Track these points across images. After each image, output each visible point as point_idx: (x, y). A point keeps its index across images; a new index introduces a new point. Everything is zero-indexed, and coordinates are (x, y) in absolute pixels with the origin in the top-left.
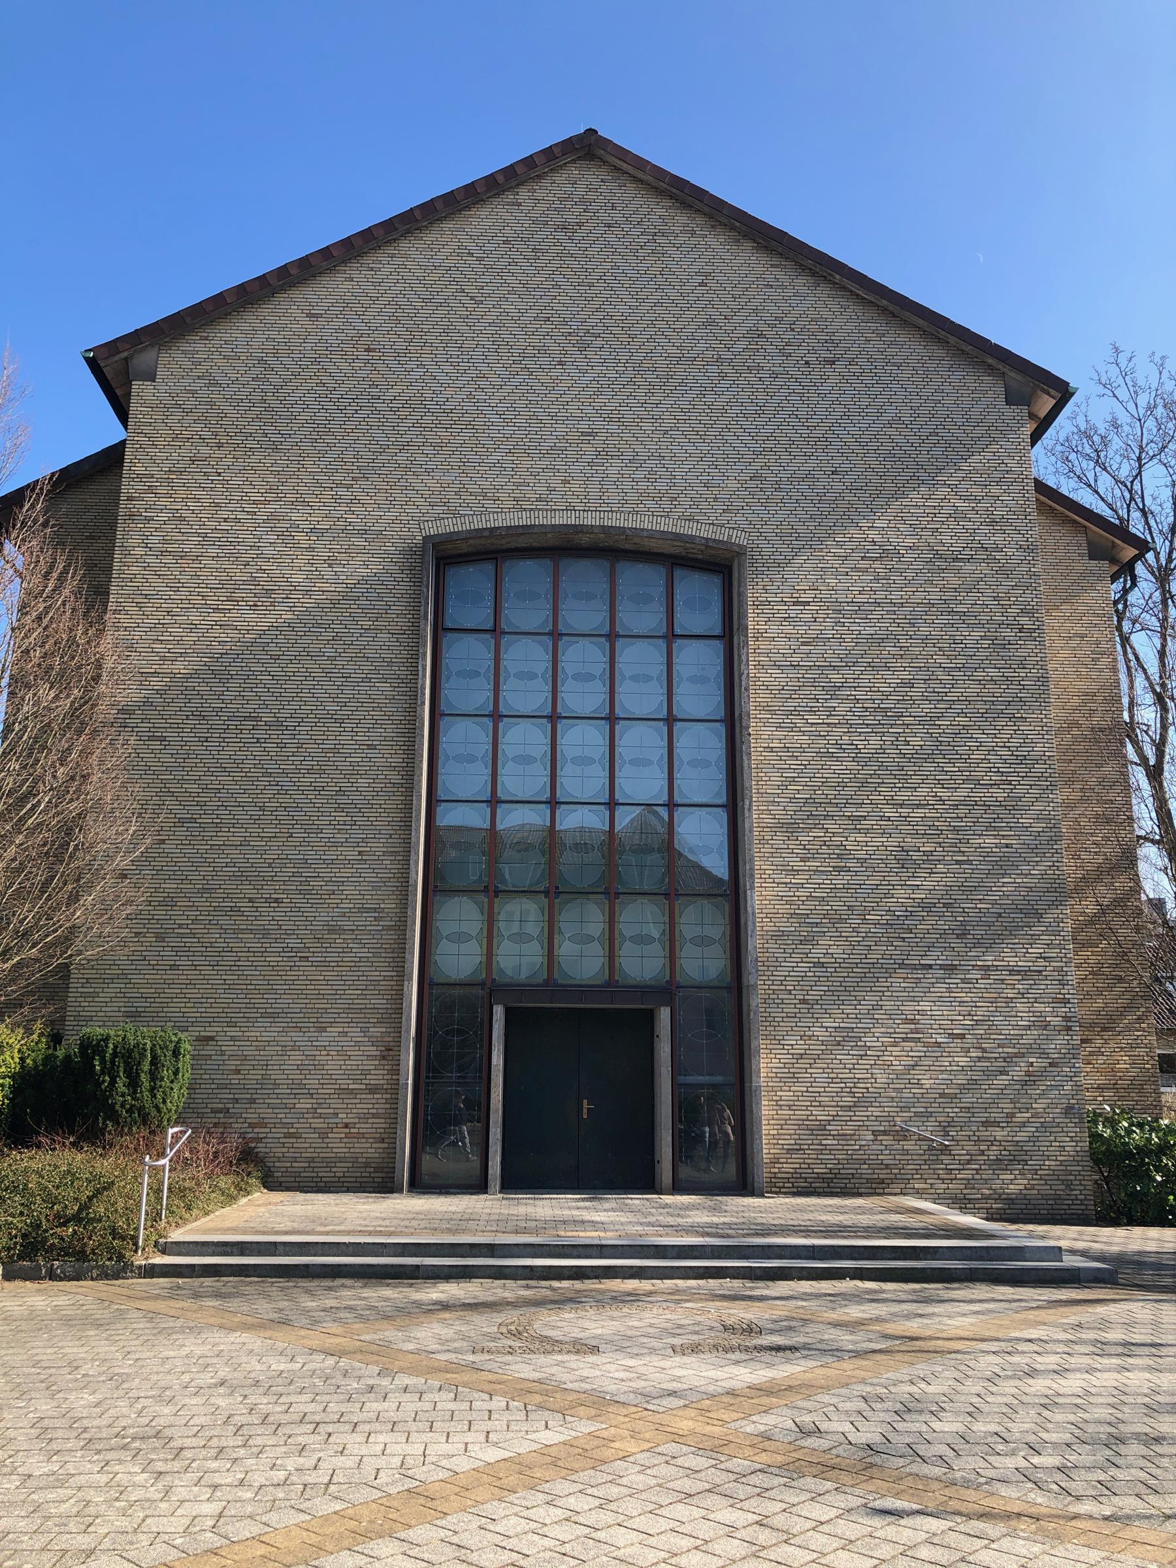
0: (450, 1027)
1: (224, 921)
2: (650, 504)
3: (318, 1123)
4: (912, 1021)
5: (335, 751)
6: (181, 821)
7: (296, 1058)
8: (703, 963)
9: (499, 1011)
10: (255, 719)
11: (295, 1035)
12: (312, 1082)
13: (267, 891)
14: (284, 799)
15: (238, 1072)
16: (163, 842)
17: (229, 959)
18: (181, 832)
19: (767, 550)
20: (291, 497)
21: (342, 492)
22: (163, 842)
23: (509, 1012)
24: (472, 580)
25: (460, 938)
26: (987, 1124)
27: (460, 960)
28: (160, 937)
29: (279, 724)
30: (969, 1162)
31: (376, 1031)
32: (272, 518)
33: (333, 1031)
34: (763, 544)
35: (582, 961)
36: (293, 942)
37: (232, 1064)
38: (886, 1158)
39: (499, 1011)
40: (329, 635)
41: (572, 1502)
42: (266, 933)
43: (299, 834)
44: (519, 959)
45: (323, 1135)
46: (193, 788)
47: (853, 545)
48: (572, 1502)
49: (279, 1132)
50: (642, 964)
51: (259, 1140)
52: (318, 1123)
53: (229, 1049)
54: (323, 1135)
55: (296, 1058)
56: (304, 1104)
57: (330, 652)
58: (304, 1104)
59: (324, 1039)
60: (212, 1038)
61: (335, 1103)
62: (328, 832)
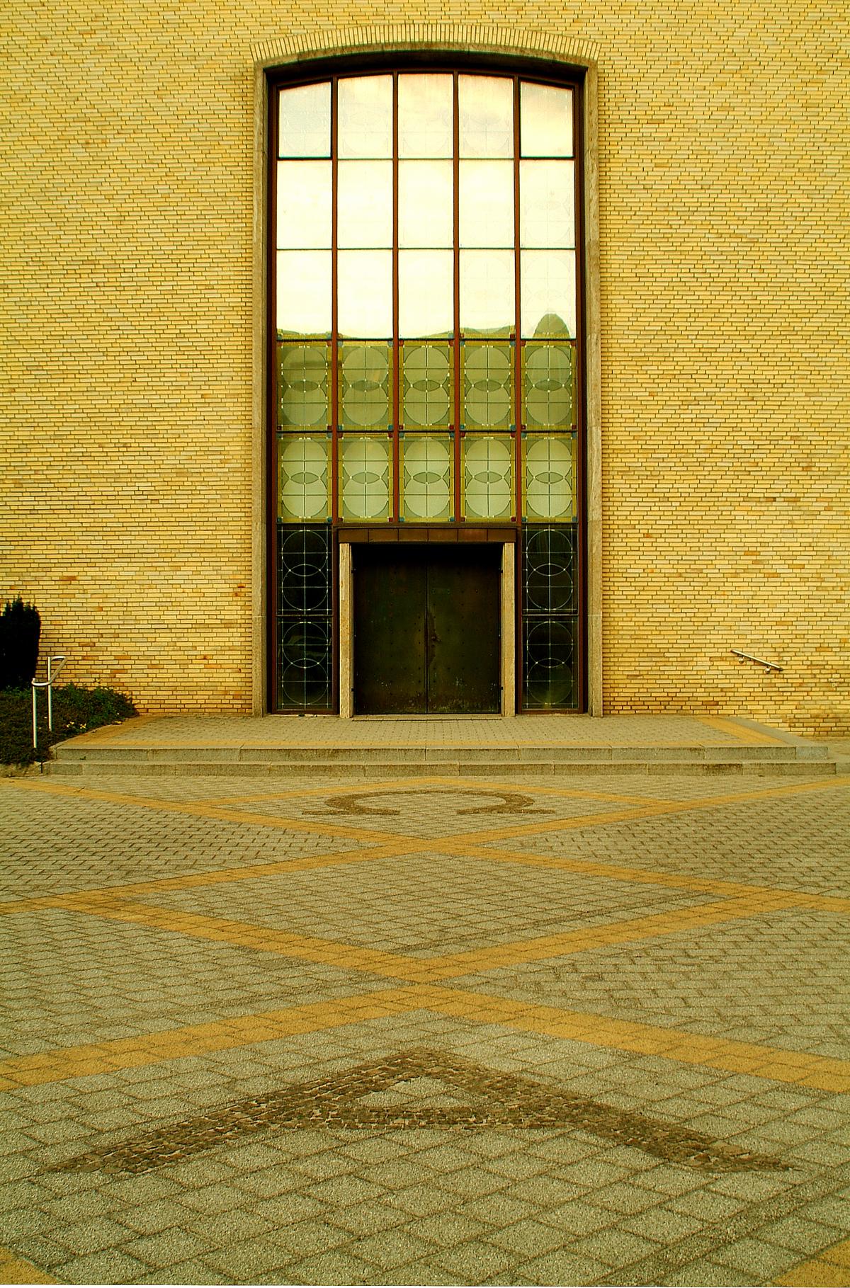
0: (295, 559)
1: (79, 467)
2: (494, 15)
3: (178, 655)
4: (753, 553)
5: (173, 293)
6: (29, 369)
7: (154, 595)
8: (551, 504)
9: (345, 551)
10: (94, 263)
11: (151, 574)
12: (171, 618)
13: (116, 436)
14: (127, 344)
15: (101, 609)
16: (14, 390)
17: (84, 502)
18: (29, 380)
19: (620, 62)
20: (117, 25)
21: (169, 15)
22: (14, 390)
23: (356, 549)
24: (302, 108)
25: (305, 478)
26: (819, 649)
27: (305, 504)
28: (18, 484)
29: (117, 268)
30: (801, 685)
31: (228, 570)
32: (101, 48)
33: (186, 571)
34: (616, 57)
35: (428, 506)
36: (143, 485)
37: (94, 603)
38: (723, 683)
39: (345, 551)
40: (161, 171)
41: (508, 1166)
42: (117, 476)
43: (142, 379)
44: (367, 505)
45: (184, 667)
46: (38, 336)
47: (712, 56)
48: (508, 1166)
49: (143, 664)
50: (489, 504)
51: (123, 671)
52: (178, 655)
53: (91, 589)
54: (184, 667)
55: (154, 595)
56: (165, 638)
57: (163, 189)
58: (165, 638)
59: (179, 577)
60: (73, 578)
61: (193, 637)
62: (171, 376)
